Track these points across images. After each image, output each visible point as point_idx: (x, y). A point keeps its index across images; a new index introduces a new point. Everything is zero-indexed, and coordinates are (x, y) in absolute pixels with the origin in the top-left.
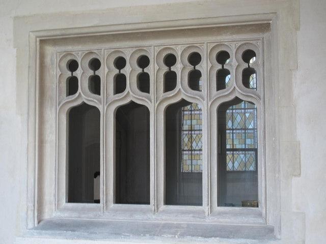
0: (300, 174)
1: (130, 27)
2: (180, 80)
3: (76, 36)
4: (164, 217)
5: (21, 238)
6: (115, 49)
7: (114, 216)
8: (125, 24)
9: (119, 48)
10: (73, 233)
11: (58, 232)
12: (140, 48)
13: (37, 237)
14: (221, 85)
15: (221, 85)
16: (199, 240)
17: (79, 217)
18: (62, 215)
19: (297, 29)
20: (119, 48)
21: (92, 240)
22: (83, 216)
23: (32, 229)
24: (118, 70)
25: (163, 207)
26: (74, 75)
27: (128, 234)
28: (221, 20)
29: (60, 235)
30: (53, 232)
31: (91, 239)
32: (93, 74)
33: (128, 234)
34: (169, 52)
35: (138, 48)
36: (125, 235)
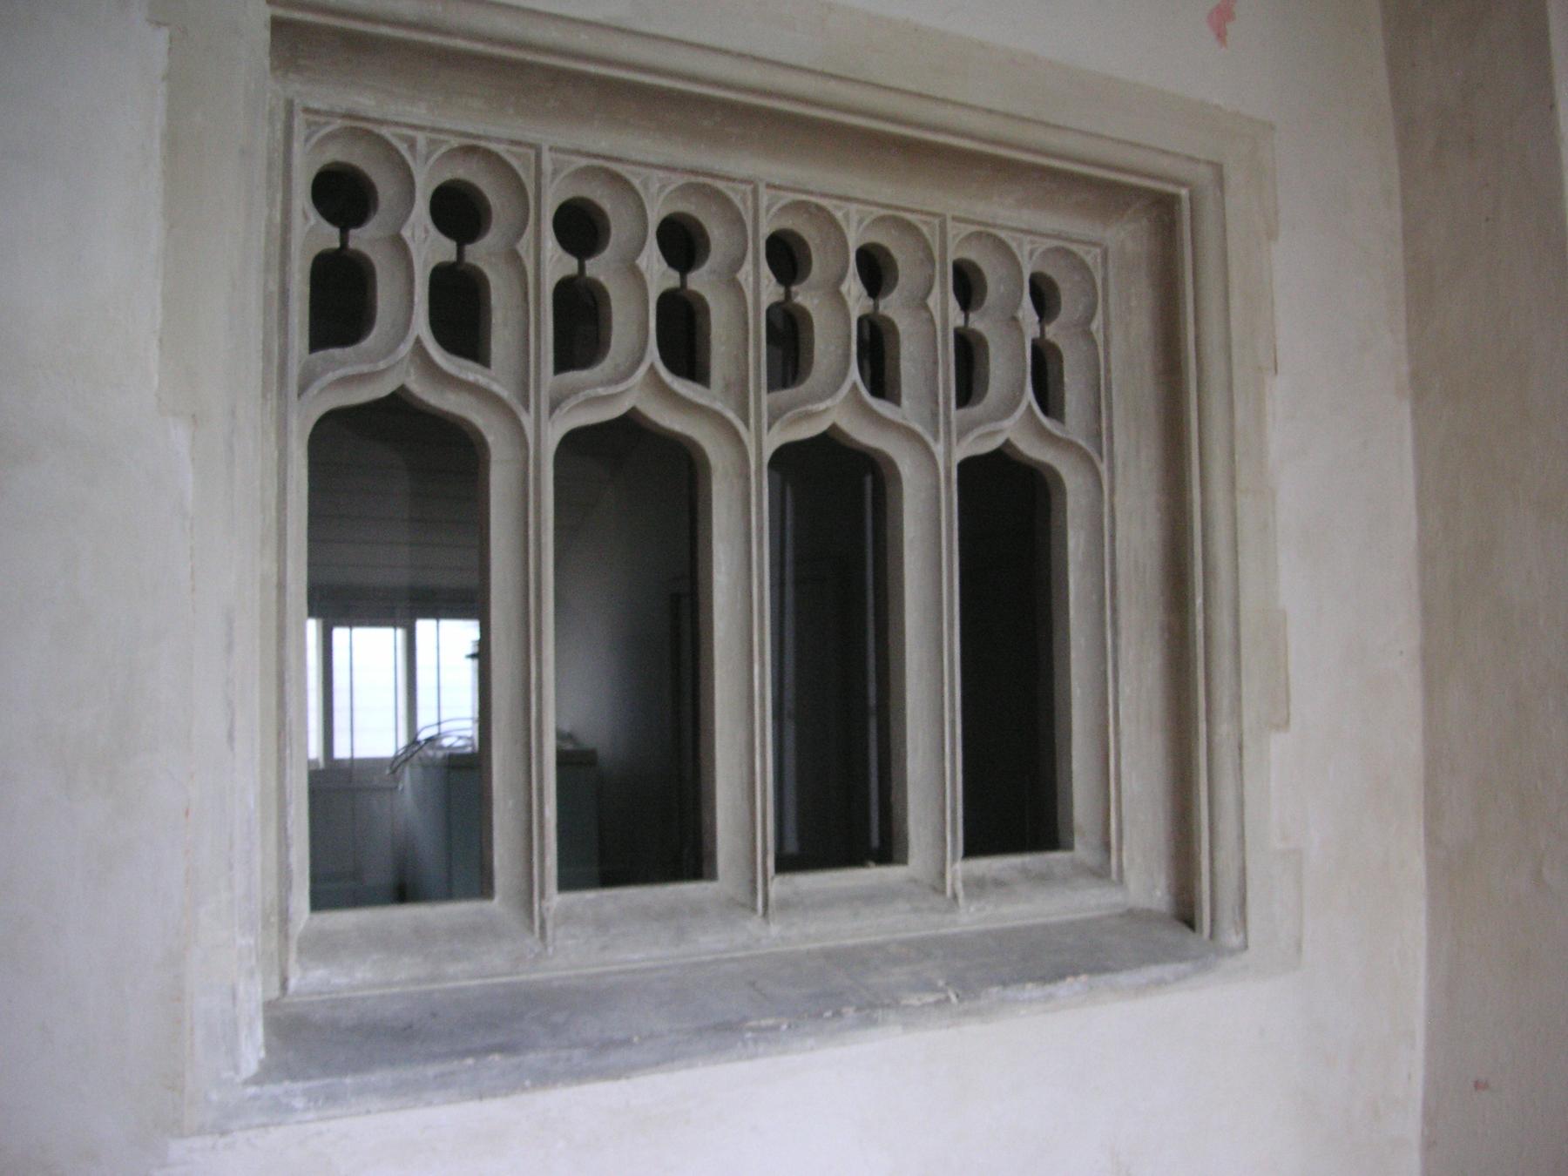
0: (1287, 722)
1: (753, 75)
2: (1193, 348)
3: (480, 47)
4: (812, 929)
5: (209, 1141)
6: (597, 156)
7: (604, 948)
8: (741, 56)
9: (618, 160)
10: (514, 1060)
11: (431, 1070)
12: (709, 181)
13: (311, 1115)
14: (969, 386)
15: (969, 386)
16: (1026, 995)
17: (433, 979)
18: (340, 980)
19: (1272, 235)
20: (618, 160)
21: (618, 1077)
22: (452, 969)
23: (257, 1080)
24: (353, 244)
25: (960, 869)
26: (352, 244)
27: (770, 1022)
28: (1073, 144)
29: (443, 1082)
30: (407, 1073)
31: (603, 1074)
32: (337, 245)
33: (770, 1022)
34: (606, 205)
35: (693, 179)
36: (759, 1030)
